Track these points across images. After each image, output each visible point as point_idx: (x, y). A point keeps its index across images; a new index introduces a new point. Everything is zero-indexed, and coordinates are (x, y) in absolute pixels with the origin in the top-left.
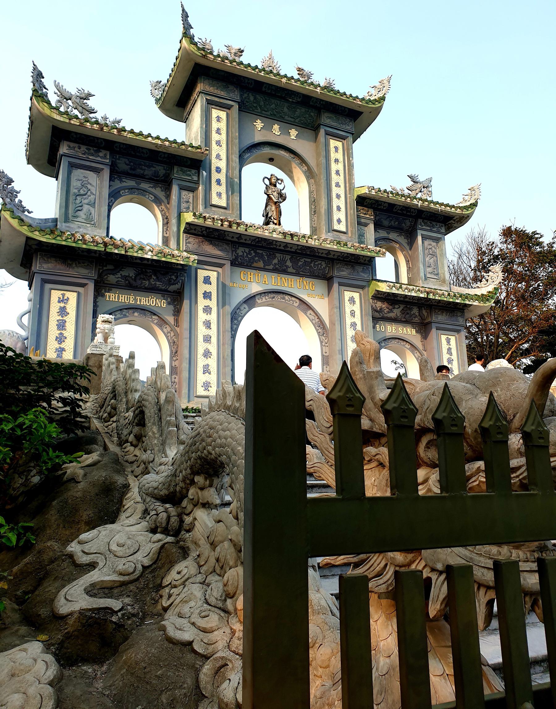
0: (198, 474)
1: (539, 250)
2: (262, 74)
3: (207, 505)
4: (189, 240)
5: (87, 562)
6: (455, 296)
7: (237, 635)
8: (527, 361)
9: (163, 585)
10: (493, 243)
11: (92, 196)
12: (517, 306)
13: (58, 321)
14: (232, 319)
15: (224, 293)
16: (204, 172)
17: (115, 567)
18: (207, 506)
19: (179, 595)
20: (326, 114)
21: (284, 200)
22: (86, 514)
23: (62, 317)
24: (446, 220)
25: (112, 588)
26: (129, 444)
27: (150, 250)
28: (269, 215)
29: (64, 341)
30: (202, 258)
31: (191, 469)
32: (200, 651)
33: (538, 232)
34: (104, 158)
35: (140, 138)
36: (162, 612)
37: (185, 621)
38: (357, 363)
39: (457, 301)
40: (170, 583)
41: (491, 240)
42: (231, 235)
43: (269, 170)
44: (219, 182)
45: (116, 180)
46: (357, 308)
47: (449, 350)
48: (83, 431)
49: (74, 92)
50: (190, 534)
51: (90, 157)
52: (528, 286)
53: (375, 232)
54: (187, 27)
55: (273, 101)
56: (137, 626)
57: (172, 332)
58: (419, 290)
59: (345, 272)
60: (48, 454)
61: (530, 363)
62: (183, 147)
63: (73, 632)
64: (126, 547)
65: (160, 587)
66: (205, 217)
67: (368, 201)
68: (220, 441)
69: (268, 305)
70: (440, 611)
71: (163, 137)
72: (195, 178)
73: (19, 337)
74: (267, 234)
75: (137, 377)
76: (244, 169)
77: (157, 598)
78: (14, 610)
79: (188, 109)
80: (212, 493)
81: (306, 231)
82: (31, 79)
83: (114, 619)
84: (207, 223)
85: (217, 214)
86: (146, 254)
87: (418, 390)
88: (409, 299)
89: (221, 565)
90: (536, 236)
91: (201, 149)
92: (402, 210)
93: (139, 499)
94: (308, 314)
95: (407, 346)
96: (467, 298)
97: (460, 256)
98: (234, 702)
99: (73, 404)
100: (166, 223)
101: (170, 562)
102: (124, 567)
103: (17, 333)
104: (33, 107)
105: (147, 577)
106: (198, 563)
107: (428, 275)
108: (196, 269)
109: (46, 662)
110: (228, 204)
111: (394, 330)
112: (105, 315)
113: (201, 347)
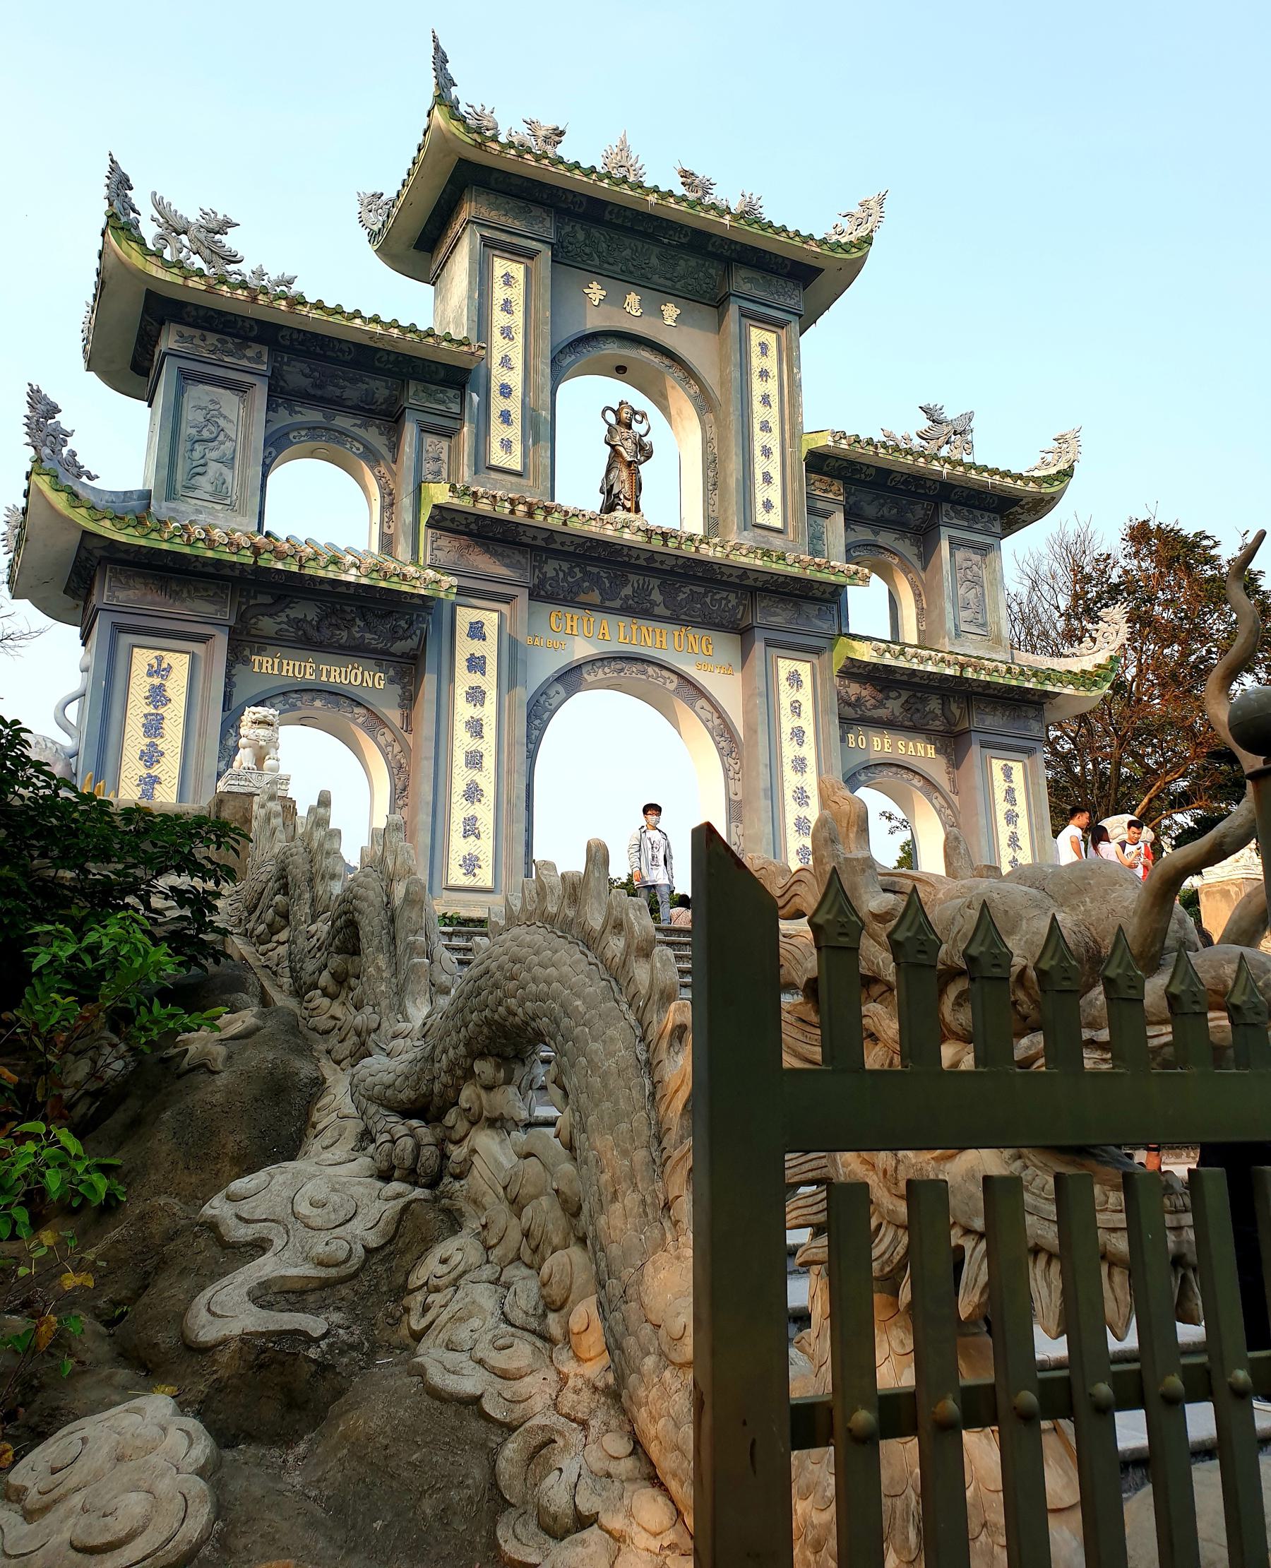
0: (482, 1055)
1: (1209, 573)
2: (605, 184)
3: (497, 1123)
4: (440, 542)
5: (249, 1239)
6: (1022, 673)
7: (571, 1383)
8: (1184, 819)
9: (410, 1287)
10: (1109, 556)
11: (228, 444)
12: (1161, 696)
13: (146, 716)
14: (529, 716)
15: (513, 658)
16: (474, 395)
17: (307, 1248)
18: (498, 1124)
19: (445, 1306)
20: (744, 273)
21: (648, 457)
22: (234, 1139)
23: (156, 707)
24: (1006, 506)
25: (303, 1292)
26: (319, 992)
27: (354, 565)
28: (615, 491)
29: (158, 762)
30: (468, 583)
31: (467, 1044)
32: (497, 1414)
33: (1208, 534)
34: (255, 361)
35: (337, 319)
36: (409, 1341)
37: (464, 1357)
38: (826, 841)
39: (1027, 685)
40: (426, 1283)
41: (1104, 550)
42: (530, 533)
43: (616, 391)
44: (506, 417)
45: (281, 409)
46: (805, 696)
47: (1010, 791)
48: (217, 962)
49: (193, 216)
50: (462, 1182)
51: (226, 359)
52: (1185, 654)
53: (846, 530)
54: (444, 82)
55: (627, 241)
56: (362, 1368)
57: (396, 744)
58: (942, 660)
59: (780, 617)
60: (150, 1011)
61: (1192, 824)
62: (431, 340)
63: (229, 1378)
64: (329, 1207)
65: (404, 1290)
66: (475, 493)
67: (833, 462)
68: (534, 987)
69: (608, 687)
70: (978, 1306)
71: (386, 318)
72: (455, 408)
73: (59, 749)
74: (609, 531)
75: (336, 846)
76: (563, 389)
77: (398, 1314)
78: (98, 1335)
79: (441, 255)
80: (511, 1097)
81: (695, 525)
82: (105, 191)
83: (313, 1353)
84: (479, 506)
85: (503, 488)
86: (346, 572)
87: (941, 895)
88: (921, 678)
89: (533, 1244)
90: (1205, 543)
91: (469, 344)
92: (906, 482)
93: (350, 1109)
94: (697, 708)
95: (917, 782)
96: (1048, 678)
97: (1035, 585)
98: (570, 1512)
99: (201, 903)
100: (389, 504)
101: (423, 1240)
102: (327, 1248)
103: (54, 743)
104: (107, 250)
105: (376, 1271)
106: (484, 1242)
107: (964, 627)
108: (453, 607)
109: (188, 1433)
110: (525, 465)
111: (886, 745)
112: (259, 709)
113: (460, 777)
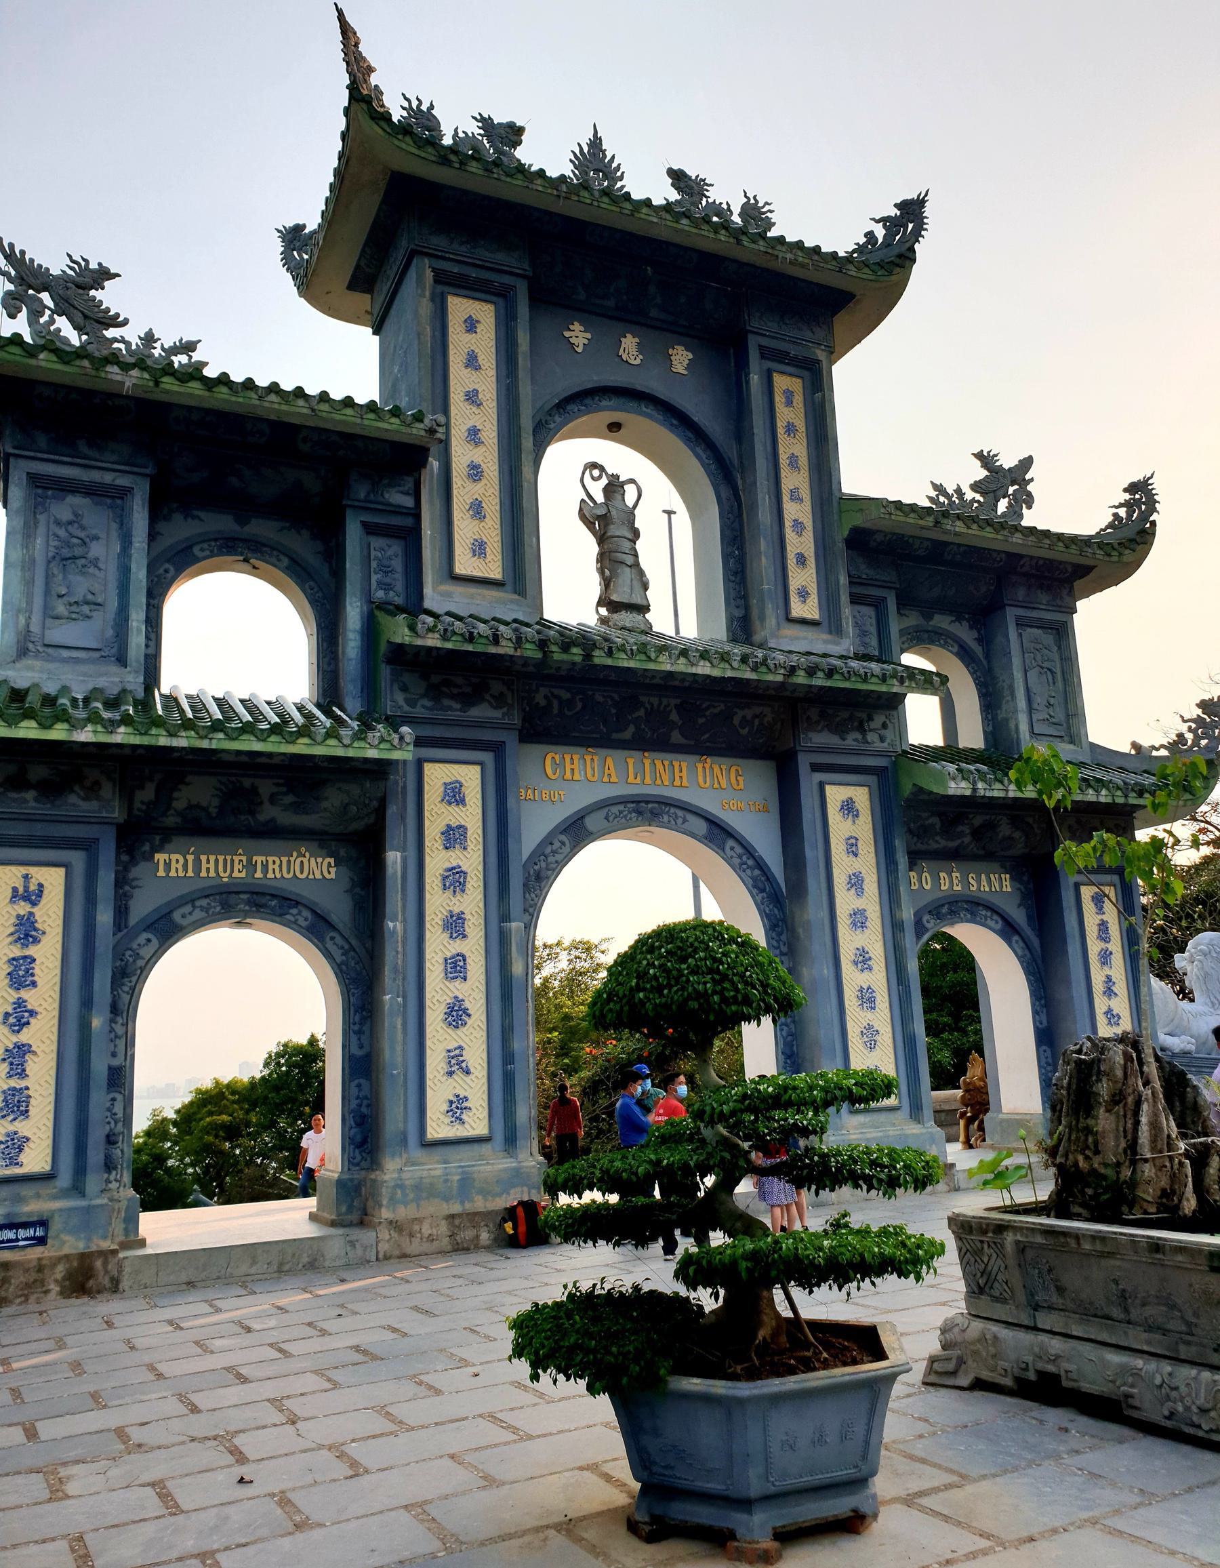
29: (28, 1023)
30: (427, 732)
47: (1103, 926)
49: (57, 266)
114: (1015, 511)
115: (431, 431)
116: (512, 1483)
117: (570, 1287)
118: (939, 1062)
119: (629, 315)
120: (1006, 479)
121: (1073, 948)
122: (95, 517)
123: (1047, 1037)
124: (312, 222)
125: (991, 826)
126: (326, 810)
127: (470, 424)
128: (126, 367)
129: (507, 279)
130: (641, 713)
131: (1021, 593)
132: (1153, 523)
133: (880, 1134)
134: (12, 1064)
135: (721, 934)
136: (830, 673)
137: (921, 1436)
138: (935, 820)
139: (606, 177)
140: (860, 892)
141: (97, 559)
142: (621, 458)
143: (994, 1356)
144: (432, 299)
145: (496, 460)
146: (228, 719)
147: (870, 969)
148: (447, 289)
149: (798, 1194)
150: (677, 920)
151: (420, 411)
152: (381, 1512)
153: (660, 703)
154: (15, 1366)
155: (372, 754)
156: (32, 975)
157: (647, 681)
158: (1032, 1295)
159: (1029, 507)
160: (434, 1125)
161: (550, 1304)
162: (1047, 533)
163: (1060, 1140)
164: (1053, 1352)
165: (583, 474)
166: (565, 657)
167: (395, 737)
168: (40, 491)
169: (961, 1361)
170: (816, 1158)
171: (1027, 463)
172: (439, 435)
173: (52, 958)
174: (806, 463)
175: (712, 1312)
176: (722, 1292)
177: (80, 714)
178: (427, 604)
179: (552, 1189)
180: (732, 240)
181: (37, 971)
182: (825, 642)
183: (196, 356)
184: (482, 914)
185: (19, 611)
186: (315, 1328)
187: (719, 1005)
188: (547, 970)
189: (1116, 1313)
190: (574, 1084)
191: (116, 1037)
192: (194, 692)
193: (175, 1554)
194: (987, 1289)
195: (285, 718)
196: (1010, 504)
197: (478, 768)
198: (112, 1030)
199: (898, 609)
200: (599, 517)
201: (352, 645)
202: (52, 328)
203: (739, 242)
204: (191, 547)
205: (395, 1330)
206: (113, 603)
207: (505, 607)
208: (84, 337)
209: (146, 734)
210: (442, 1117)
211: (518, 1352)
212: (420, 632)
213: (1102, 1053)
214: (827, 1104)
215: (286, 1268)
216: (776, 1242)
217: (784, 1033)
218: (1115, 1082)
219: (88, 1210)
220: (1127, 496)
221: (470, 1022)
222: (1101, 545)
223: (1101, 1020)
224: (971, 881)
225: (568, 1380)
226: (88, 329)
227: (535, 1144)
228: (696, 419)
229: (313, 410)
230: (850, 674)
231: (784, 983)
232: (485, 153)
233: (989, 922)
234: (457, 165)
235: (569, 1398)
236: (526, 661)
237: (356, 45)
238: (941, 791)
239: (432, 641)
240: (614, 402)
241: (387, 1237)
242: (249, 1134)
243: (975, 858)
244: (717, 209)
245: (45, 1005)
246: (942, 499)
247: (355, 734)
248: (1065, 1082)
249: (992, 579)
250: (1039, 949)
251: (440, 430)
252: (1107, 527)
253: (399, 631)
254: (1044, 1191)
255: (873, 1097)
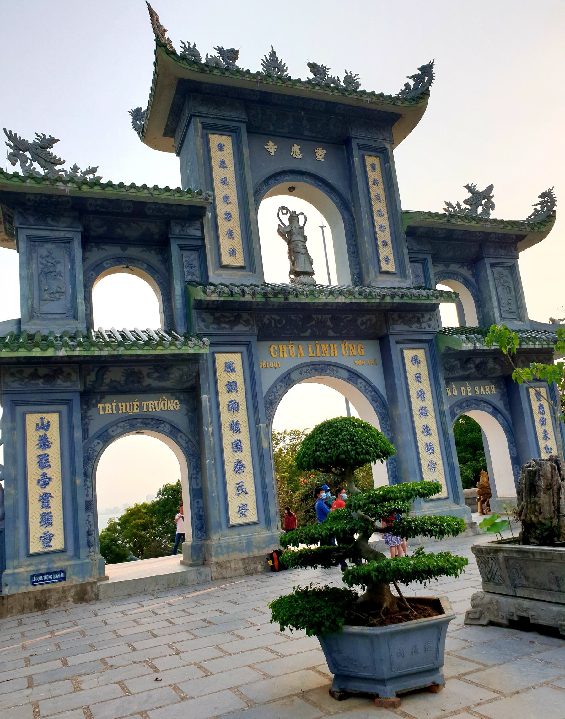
29: (48, 484)
47: (541, 407)
49: (31, 139)
54: (159, 30)
114: (486, 212)
115: (206, 199)
116: (277, 676)
117: (296, 588)
118: (467, 476)
119: (295, 135)
120: (481, 197)
121: (527, 419)
122: (58, 252)
123: (517, 461)
124: (144, 106)
125: (484, 363)
126: (173, 379)
127: (224, 194)
128: (65, 182)
129: (236, 124)
130: (313, 323)
131: (492, 251)
132: (555, 212)
133: (440, 511)
134: (43, 502)
135: (353, 423)
136: (402, 296)
137: (464, 648)
138: (457, 362)
139: (279, 70)
140: (423, 399)
141: (60, 272)
142: (296, 203)
143: (497, 610)
144: (202, 137)
145: (238, 210)
146: (125, 340)
147: (430, 434)
148: (208, 131)
149: (403, 540)
150: (332, 418)
151: (200, 190)
152: (219, 691)
153: (322, 317)
154: (56, 634)
155: (191, 351)
156: (48, 462)
157: (315, 308)
158: (514, 581)
159: (493, 210)
160: (233, 518)
161: (288, 596)
162: (502, 221)
163: (523, 509)
164: (525, 607)
165: (279, 212)
166: (276, 300)
167: (201, 343)
168: (32, 243)
169: (482, 613)
170: (405, 523)
171: (490, 188)
172: (210, 201)
173: (56, 454)
174: (384, 197)
175: (362, 596)
176: (366, 587)
177: (59, 343)
178: (211, 280)
179: (284, 544)
180: (340, 94)
181: (50, 460)
182: (399, 282)
183: (97, 174)
184: (247, 421)
185: (28, 299)
186: (185, 612)
187: (355, 456)
188: (280, 445)
189: (555, 587)
190: (297, 496)
191: (88, 487)
192: (109, 329)
193: (129, 713)
194: (492, 580)
195: (151, 339)
196: (483, 209)
197: (240, 355)
198: (85, 484)
199: (433, 263)
200: (287, 232)
201: (178, 302)
202: (32, 168)
203: (344, 95)
204: (102, 263)
205: (221, 611)
206: (69, 292)
207: (247, 279)
208: (46, 171)
209: (89, 350)
210: (236, 514)
211: (274, 618)
212: (208, 294)
213: (540, 466)
214: (409, 498)
215: (171, 586)
216: (388, 562)
217: (391, 467)
218: (547, 480)
219: (82, 564)
220: (541, 200)
221: (245, 470)
222: (529, 225)
223: (543, 451)
224: (476, 390)
225: (297, 630)
226: (48, 167)
227: (280, 524)
228: (330, 181)
229: (152, 194)
230: (412, 296)
231: (385, 444)
232: (221, 65)
233: (486, 409)
234: (208, 72)
235: (300, 638)
236: (258, 303)
237: (157, 20)
238: (458, 348)
239: (214, 297)
240: (291, 177)
241: (216, 570)
242: (152, 527)
243: (476, 379)
244: (333, 80)
245: (55, 475)
246: (450, 209)
247: (183, 343)
248: (524, 481)
249: (476, 245)
250: (511, 421)
251: (210, 198)
252: (532, 215)
253: (199, 294)
254: (516, 534)
255: (430, 493)
